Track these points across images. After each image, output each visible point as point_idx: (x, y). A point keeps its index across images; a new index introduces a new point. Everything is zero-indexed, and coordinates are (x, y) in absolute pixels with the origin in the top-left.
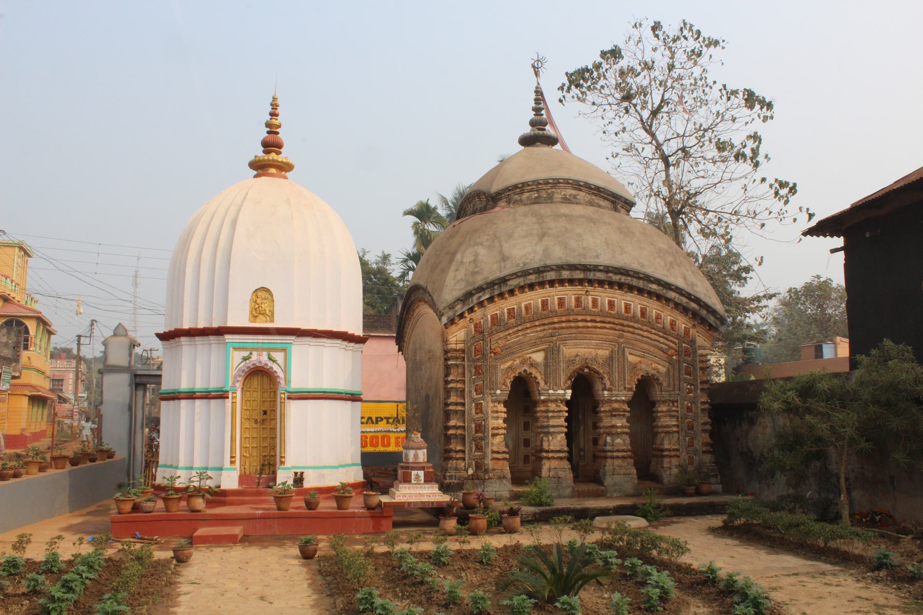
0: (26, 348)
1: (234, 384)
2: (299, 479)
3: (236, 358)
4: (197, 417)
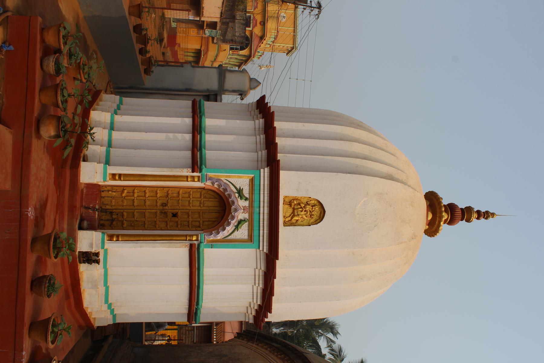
0: (231, 49)
1: (210, 179)
2: (90, 258)
3: (241, 181)
4: (171, 135)
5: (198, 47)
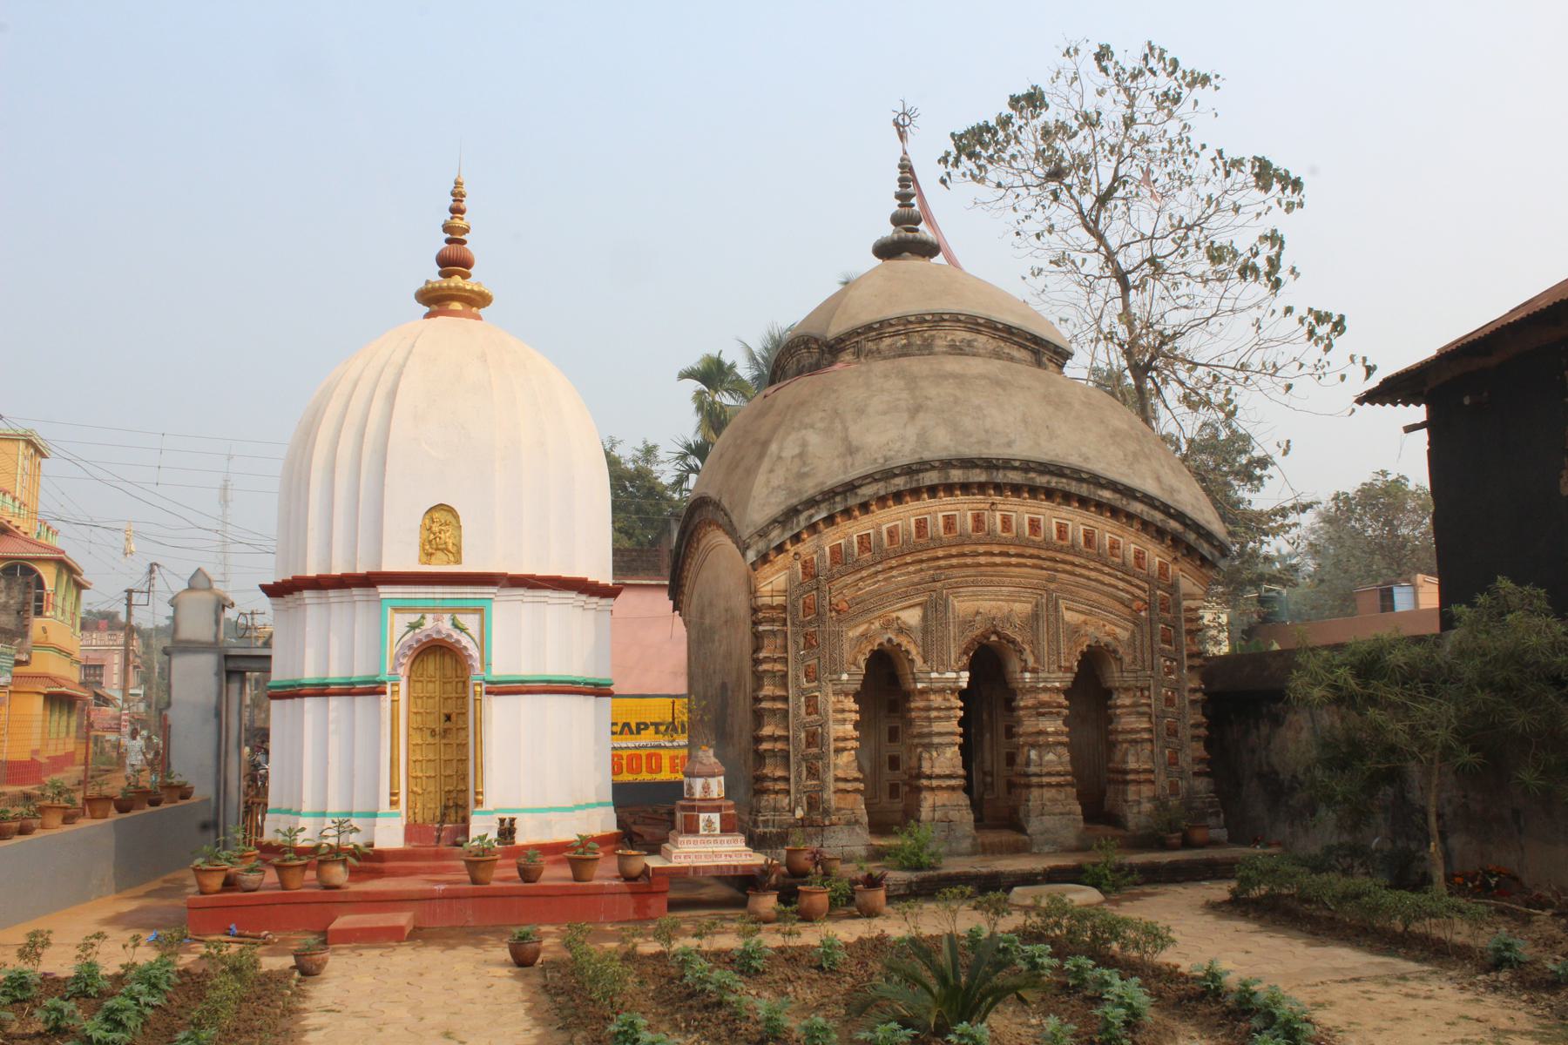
0: (39, 612)
1: (394, 669)
2: (507, 831)
3: (398, 625)
4: (332, 727)
5: (41, 698)
